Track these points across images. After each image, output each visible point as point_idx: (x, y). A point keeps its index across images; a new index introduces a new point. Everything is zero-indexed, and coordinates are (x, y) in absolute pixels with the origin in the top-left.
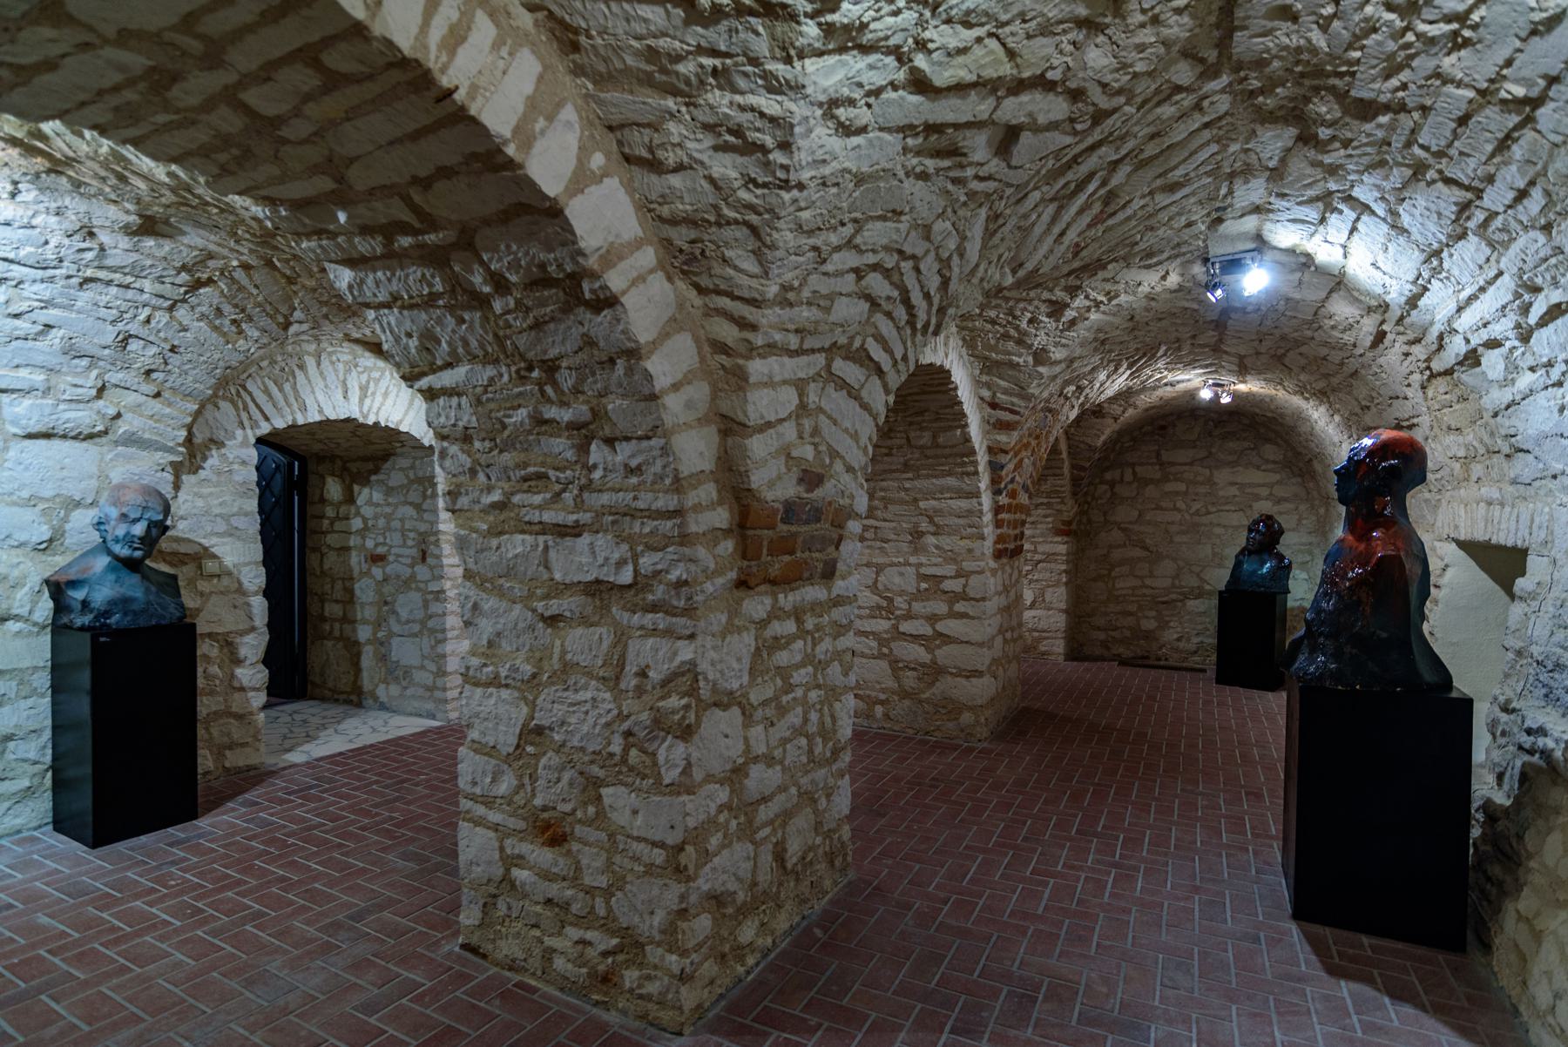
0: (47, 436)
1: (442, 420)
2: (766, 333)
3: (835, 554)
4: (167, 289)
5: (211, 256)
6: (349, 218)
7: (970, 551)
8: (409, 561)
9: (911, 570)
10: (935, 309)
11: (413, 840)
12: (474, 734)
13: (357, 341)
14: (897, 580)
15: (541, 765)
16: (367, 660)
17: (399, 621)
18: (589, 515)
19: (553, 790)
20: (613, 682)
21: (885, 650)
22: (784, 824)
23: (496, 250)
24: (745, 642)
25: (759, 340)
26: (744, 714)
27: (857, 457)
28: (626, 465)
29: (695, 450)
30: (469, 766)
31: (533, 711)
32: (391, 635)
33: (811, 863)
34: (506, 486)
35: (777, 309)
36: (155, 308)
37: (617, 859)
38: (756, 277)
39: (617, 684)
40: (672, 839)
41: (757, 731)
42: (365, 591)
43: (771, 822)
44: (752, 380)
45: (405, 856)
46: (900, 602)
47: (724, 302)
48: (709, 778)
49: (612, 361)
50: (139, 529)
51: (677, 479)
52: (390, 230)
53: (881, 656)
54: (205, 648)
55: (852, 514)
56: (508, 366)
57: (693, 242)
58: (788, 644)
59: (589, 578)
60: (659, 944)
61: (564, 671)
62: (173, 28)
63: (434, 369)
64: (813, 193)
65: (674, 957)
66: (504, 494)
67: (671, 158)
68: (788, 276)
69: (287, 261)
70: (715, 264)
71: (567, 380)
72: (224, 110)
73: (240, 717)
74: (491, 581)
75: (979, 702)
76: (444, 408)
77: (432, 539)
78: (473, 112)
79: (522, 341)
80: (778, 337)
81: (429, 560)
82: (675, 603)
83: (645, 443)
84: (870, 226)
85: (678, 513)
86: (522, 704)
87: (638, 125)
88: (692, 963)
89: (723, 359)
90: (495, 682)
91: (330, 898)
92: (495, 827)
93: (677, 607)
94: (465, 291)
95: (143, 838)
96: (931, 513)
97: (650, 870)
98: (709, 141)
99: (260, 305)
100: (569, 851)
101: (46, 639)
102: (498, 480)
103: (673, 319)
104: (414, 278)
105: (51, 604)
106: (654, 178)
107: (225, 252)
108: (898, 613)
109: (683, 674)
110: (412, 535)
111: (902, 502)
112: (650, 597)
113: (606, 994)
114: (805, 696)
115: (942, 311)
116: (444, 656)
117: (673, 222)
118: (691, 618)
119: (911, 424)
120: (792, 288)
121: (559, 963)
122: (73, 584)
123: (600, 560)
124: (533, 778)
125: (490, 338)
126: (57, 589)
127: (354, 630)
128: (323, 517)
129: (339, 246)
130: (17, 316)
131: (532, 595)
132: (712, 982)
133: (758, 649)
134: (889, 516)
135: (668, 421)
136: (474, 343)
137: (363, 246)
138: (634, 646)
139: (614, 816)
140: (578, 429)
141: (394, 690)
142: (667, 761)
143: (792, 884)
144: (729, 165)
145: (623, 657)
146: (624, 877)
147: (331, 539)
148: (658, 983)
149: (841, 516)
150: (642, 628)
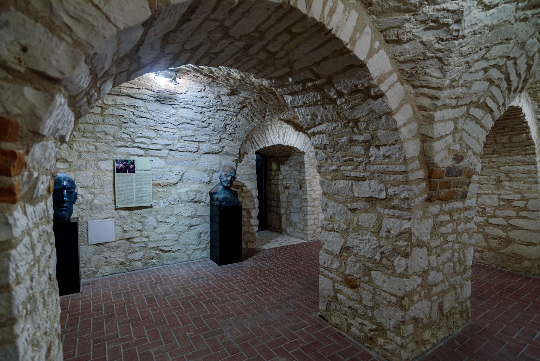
0: (209, 153)
1: (317, 142)
2: (443, 101)
3: (467, 189)
4: (236, 110)
5: (246, 99)
6: (293, 80)
7: (529, 189)
8: (296, 189)
10: (522, 80)
11: (301, 278)
12: (325, 247)
13: (282, 120)
14: (488, 200)
15: (348, 260)
16: (284, 219)
17: (293, 208)
18: (369, 173)
19: (353, 269)
20: (377, 233)
22: (443, 296)
23: (340, 82)
24: (429, 223)
25: (440, 103)
26: (428, 250)
27: (478, 148)
28: (384, 155)
29: (412, 148)
30: (323, 257)
31: (346, 241)
32: (291, 212)
33: (453, 313)
34: (338, 164)
35: (448, 90)
36: (233, 116)
37: (377, 297)
38: (440, 78)
39: (378, 234)
40: (400, 294)
41: (433, 258)
42: (283, 198)
43: (437, 294)
44: (435, 120)
45: (299, 283)
46: (489, 210)
47: (425, 90)
48: (415, 273)
49: (380, 117)
50: (229, 178)
51: (405, 160)
52: (304, 82)
54: (244, 213)
55: (475, 173)
56: (341, 122)
57: (412, 68)
58: (446, 224)
59: (368, 196)
60: (392, 332)
61: (358, 228)
62: (254, 32)
63: (315, 126)
64: (469, 39)
65: (399, 338)
66: (337, 166)
67: (405, 38)
68: (454, 76)
69: (266, 97)
70: (421, 76)
71: (362, 125)
72: (262, 53)
73: (252, 234)
74: (332, 196)
75: (534, 257)
76: (318, 138)
77: (304, 182)
78: (337, 36)
79: (347, 113)
80: (448, 101)
81: (303, 189)
82: (403, 206)
83: (392, 147)
84: (494, 48)
85: (405, 172)
86: (342, 238)
87: (392, 28)
88: (406, 342)
89: (424, 113)
90: (333, 230)
91: (279, 292)
92: (332, 279)
93: (405, 208)
94: (328, 98)
95: (230, 265)
96: (507, 172)
97: (390, 303)
98: (422, 27)
99: (258, 111)
100: (358, 292)
101: (208, 208)
102: (335, 161)
103: (404, 99)
104: (311, 96)
105: (210, 198)
106: (398, 47)
107: (250, 97)
108: (488, 214)
109: (405, 233)
110: (297, 180)
111: (491, 167)
112: (393, 204)
113: (371, 344)
114: (453, 246)
115: (526, 81)
116: (307, 220)
117: (405, 62)
118: (409, 212)
119: (497, 133)
120: (455, 81)
121: (353, 329)
122: (215, 193)
123: (373, 190)
124: (346, 264)
125: (335, 113)
126: (211, 194)
127: (280, 210)
128: (271, 175)
129: (289, 89)
130: (203, 122)
131: (346, 201)
132: (413, 351)
133: (434, 225)
135: (402, 137)
136: (329, 116)
137: (296, 88)
138: (385, 221)
139: (376, 282)
140: (366, 143)
141: (291, 229)
142: (398, 265)
143: (445, 320)
144: (431, 35)
146: (379, 304)
147: (273, 182)
148: (392, 346)
149: (470, 173)
150: (389, 215)
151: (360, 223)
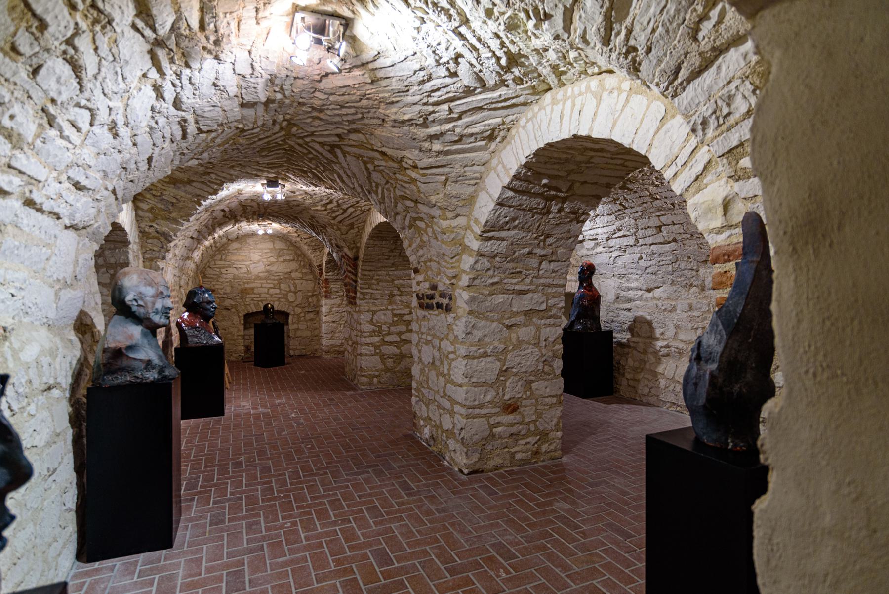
9: (389, 312)
14: (383, 317)
19: (512, 390)
20: (537, 345)
46: (384, 327)
53: (376, 354)
90: (485, 355)
92: (485, 416)
97: (552, 406)
111: (387, 281)
131: (502, 318)
138: (543, 331)
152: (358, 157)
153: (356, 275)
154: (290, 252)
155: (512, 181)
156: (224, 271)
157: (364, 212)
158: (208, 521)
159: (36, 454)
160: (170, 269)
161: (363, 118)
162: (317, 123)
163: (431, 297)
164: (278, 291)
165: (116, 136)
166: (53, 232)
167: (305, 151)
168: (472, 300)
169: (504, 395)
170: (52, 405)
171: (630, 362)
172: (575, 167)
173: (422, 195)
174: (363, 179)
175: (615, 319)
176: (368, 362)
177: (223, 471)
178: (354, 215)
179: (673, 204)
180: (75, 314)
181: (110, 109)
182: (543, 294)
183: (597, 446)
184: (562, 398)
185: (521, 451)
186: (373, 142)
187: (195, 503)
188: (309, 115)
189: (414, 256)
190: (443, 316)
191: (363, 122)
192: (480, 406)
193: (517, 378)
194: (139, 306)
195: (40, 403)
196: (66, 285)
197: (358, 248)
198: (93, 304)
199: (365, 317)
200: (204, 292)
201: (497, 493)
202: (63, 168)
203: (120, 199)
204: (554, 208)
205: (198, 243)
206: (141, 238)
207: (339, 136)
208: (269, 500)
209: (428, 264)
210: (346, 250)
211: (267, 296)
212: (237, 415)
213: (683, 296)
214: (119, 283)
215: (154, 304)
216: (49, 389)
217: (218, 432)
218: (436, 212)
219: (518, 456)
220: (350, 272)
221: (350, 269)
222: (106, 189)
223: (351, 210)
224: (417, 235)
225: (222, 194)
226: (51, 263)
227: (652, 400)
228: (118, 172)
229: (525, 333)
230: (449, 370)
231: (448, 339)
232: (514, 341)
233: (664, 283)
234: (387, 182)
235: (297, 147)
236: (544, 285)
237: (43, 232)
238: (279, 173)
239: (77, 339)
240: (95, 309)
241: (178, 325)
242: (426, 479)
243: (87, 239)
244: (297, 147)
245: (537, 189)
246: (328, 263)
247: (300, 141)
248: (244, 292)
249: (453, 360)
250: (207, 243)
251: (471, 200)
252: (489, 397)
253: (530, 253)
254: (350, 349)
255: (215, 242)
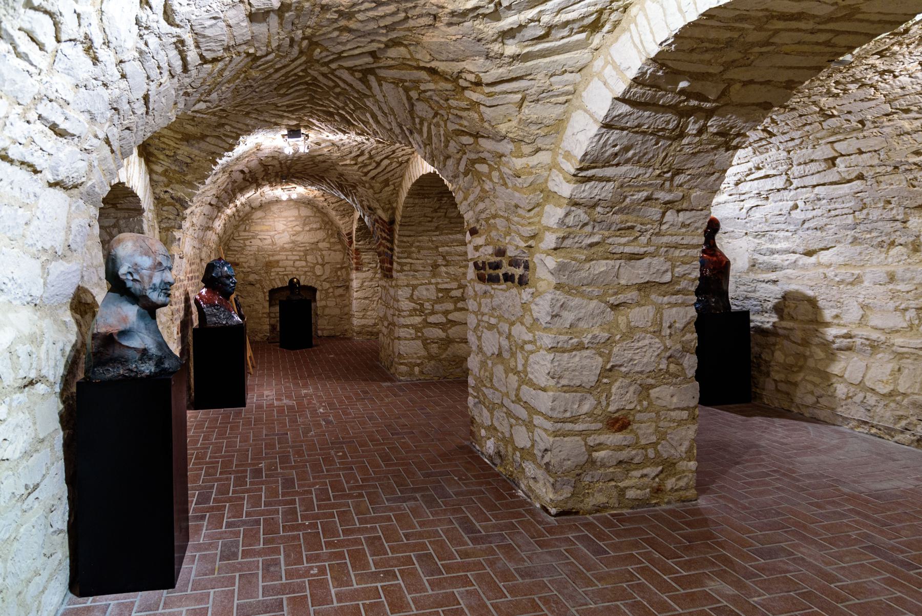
9: (433, 287)
14: (425, 293)
19: (621, 397)
20: (657, 333)
21: (419, 334)
46: (427, 305)
53: (417, 338)
83: (699, 213)
90: (580, 347)
92: (580, 433)
97: (681, 423)
111: (429, 248)
113: (657, 498)
131: (605, 294)
134: (421, 257)
138: (666, 313)
145: (661, 319)
151: (632, 324)
152: (397, 82)
153: (392, 242)
154: (317, 219)
155: (630, 87)
156: (247, 243)
157: (401, 164)
158: (219, 552)
159: (7, 469)
160: (187, 239)
161: (407, 18)
162: (346, 36)
163: (497, 266)
164: (304, 263)
165: (96, 60)
166: (30, 190)
167: (331, 84)
168: (561, 268)
169: (608, 404)
170: (35, 404)
171: (779, 356)
172: (739, 56)
173: (486, 125)
174: (403, 115)
175: (750, 295)
176: (408, 347)
177: (240, 481)
178: (389, 169)
179: (862, 122)
180: (71, 291)
181: (79, 16)
182: (667, 259)
183: (750, 484)
184: (697, 412)
185: (635, 485)
186: (418, 56)
187: (205, 523)
188: (335, 25)
189: (471, 213)
190: (514, 291)
191: (407, 25)
192: (574, 420)
193: (627, 381)
194: (134, 280)
195: (14, 404)
196: (56, 256)
197: (394, 210)
198: (95, 279)
199: (403, 293)
200: (223, 266)
201: (606, 552)
202: (29, 102)
203: (118, 152)
204: (692, 128)
205: (219, 211)
206: (156, 206)
207: (373, 54)
208: (292, 528)
209: (492, 221)
210: (380, 212)
211: (293, 269)
212: (259, 407)
213: (875, 261)
214: (113, 252)
215: (151, 278)
216: (32, 383)
217: (238, 427)
218: (506, 147)
219: (631, 494)
220: (385, 239)
221: (384, 235)
222: (96, 136)
223: (386, 162)
224: (476, 183)
225: (239, 150)
226: (32, 228)
227: (822, 414)
228: (109, 115)
229: (640, 315)
230: (525, 366)
231: (522, 324)
232: (623, 326)
233: (838, 242)
234: (436, 114)
235: (321, 78)
236: (669, 246)
237: (17, 189)
238: (301, 119)
239: (73, 321)
240: (97, 285)
241: (197, 302)
242: (496, 517)
243: (81, 202)
244: (321, 78)
245: (668, 99)
246: (358, 230)
247: (324, 69)
248: (269, 265)
249: (532, 352)
250: (229, 211)
251: (558, 126)
252: (586, 407)
253: (648, 199)
254: (385, 331)
255: (237, 211)
